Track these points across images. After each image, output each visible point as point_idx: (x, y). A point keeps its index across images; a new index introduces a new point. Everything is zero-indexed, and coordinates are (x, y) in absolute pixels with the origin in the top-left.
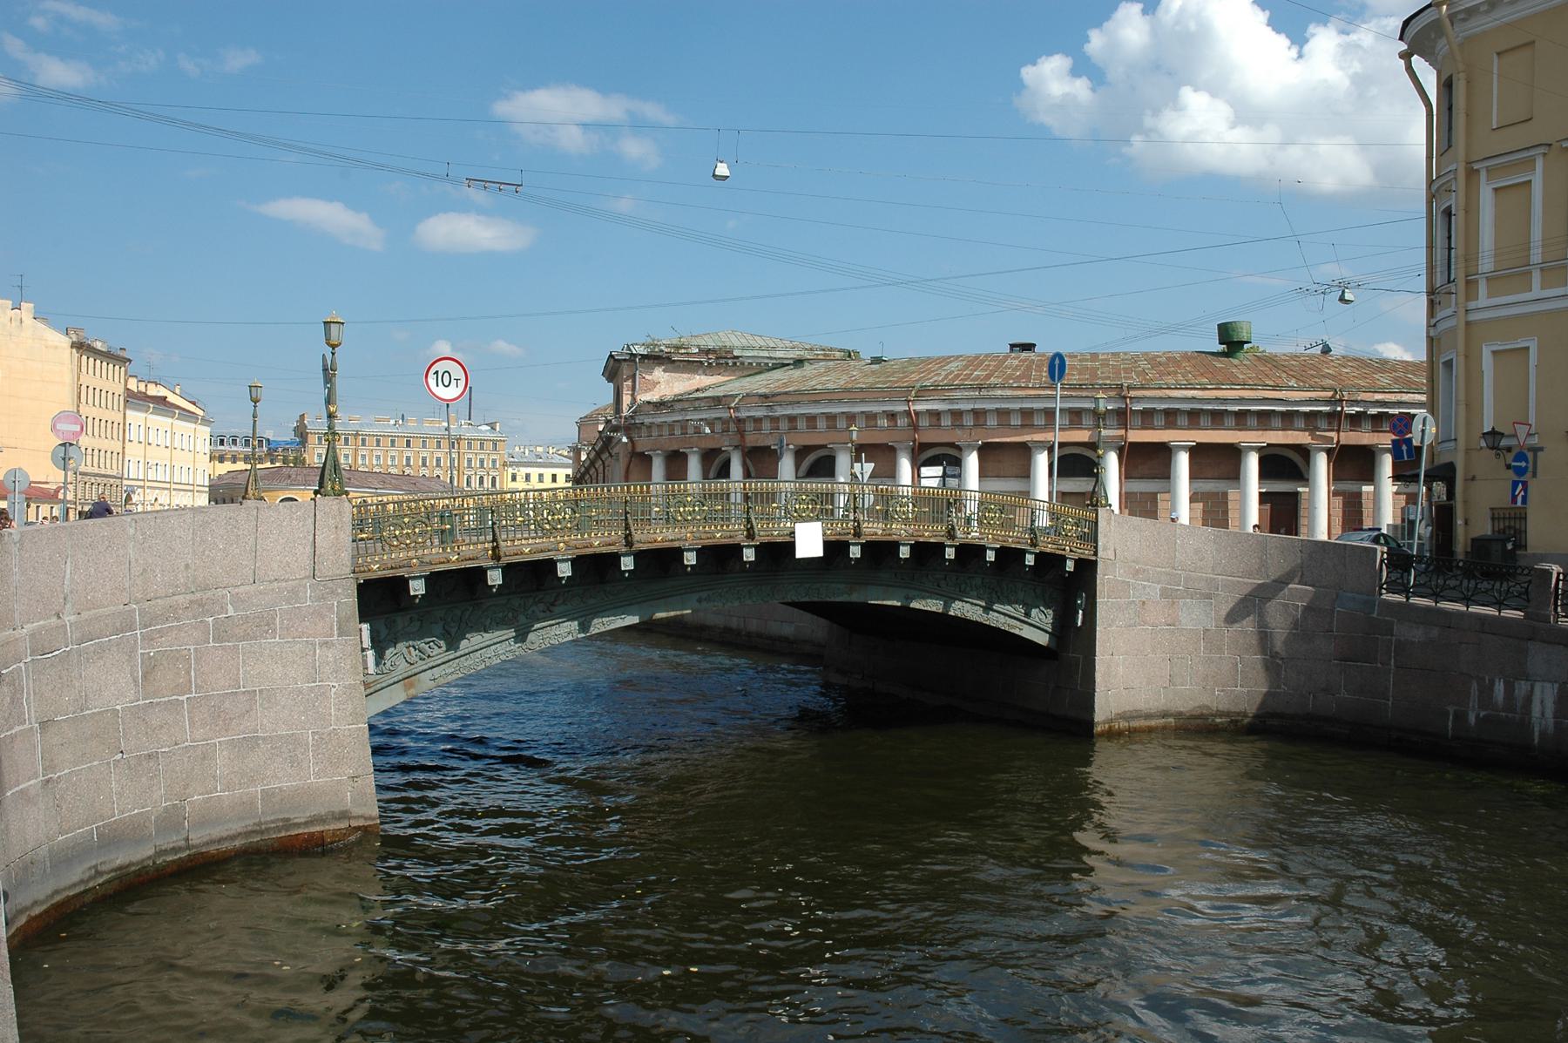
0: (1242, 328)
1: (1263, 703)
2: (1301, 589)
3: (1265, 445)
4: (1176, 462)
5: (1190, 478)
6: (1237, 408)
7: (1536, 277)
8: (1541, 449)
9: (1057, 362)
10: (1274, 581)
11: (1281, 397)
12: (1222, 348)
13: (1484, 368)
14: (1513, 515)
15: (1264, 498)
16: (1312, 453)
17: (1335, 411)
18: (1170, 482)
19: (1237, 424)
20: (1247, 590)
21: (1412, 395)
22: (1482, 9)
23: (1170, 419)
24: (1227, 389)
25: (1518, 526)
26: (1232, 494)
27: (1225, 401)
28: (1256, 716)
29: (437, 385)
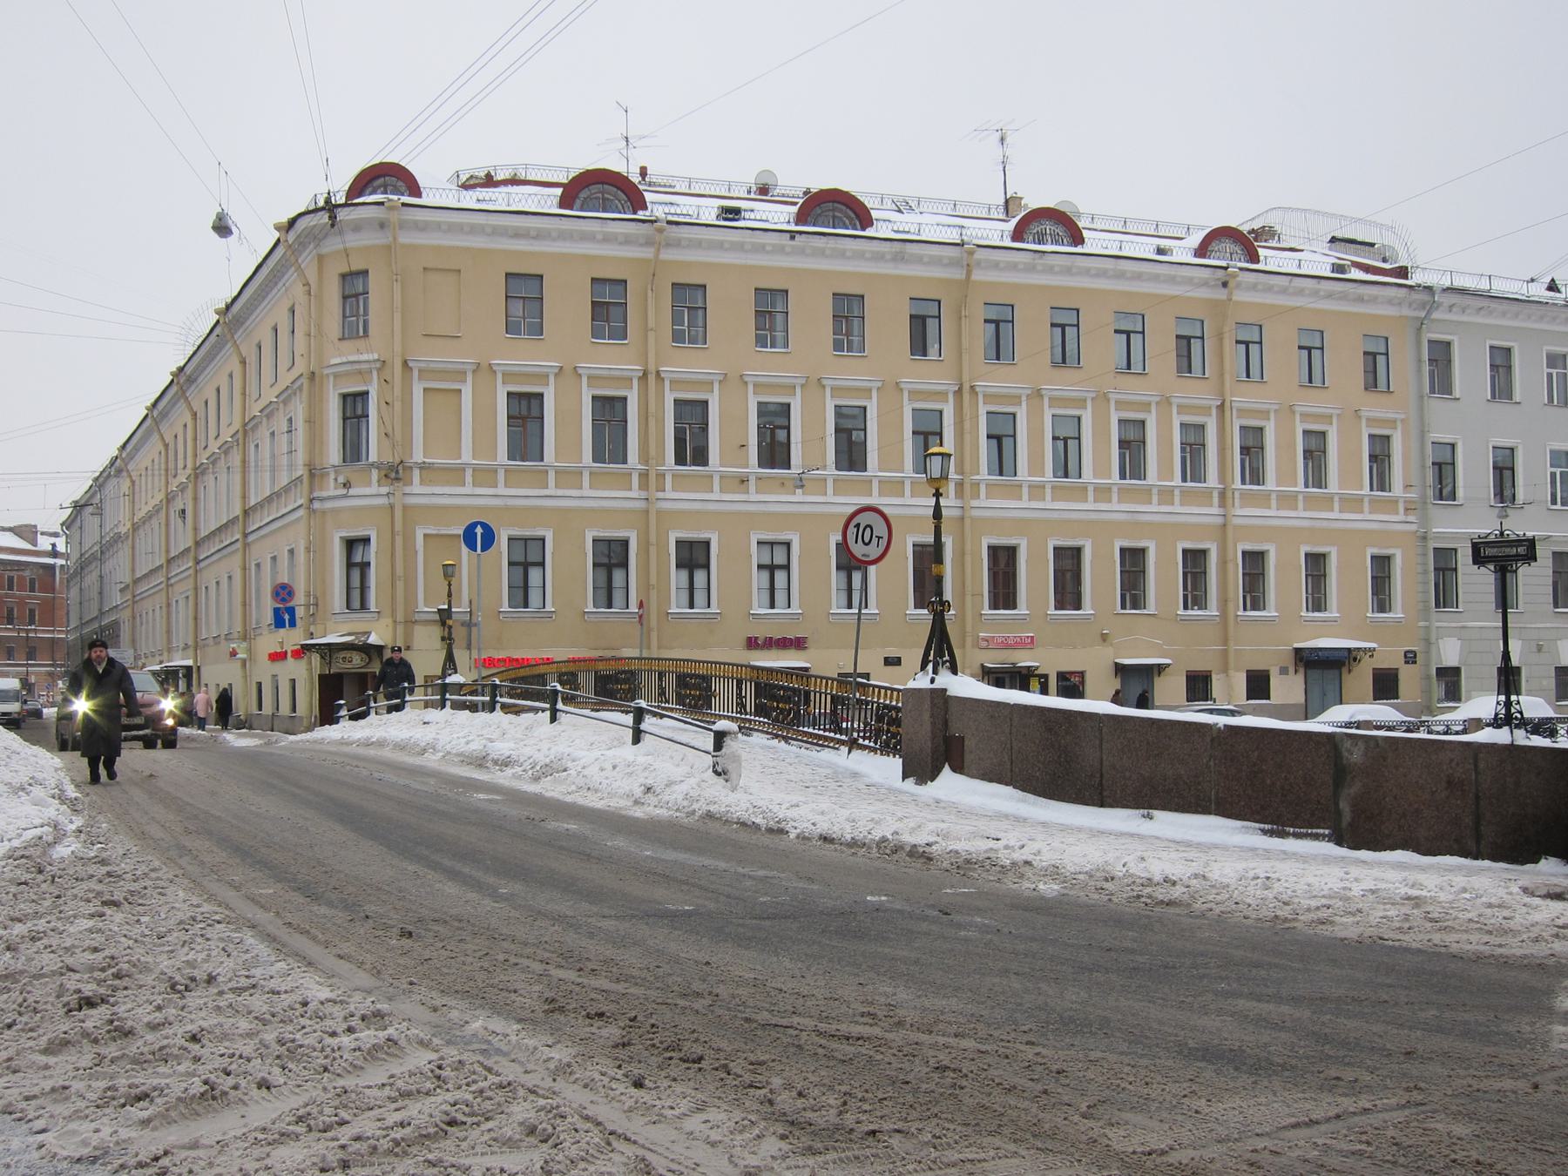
9: (479, 530)
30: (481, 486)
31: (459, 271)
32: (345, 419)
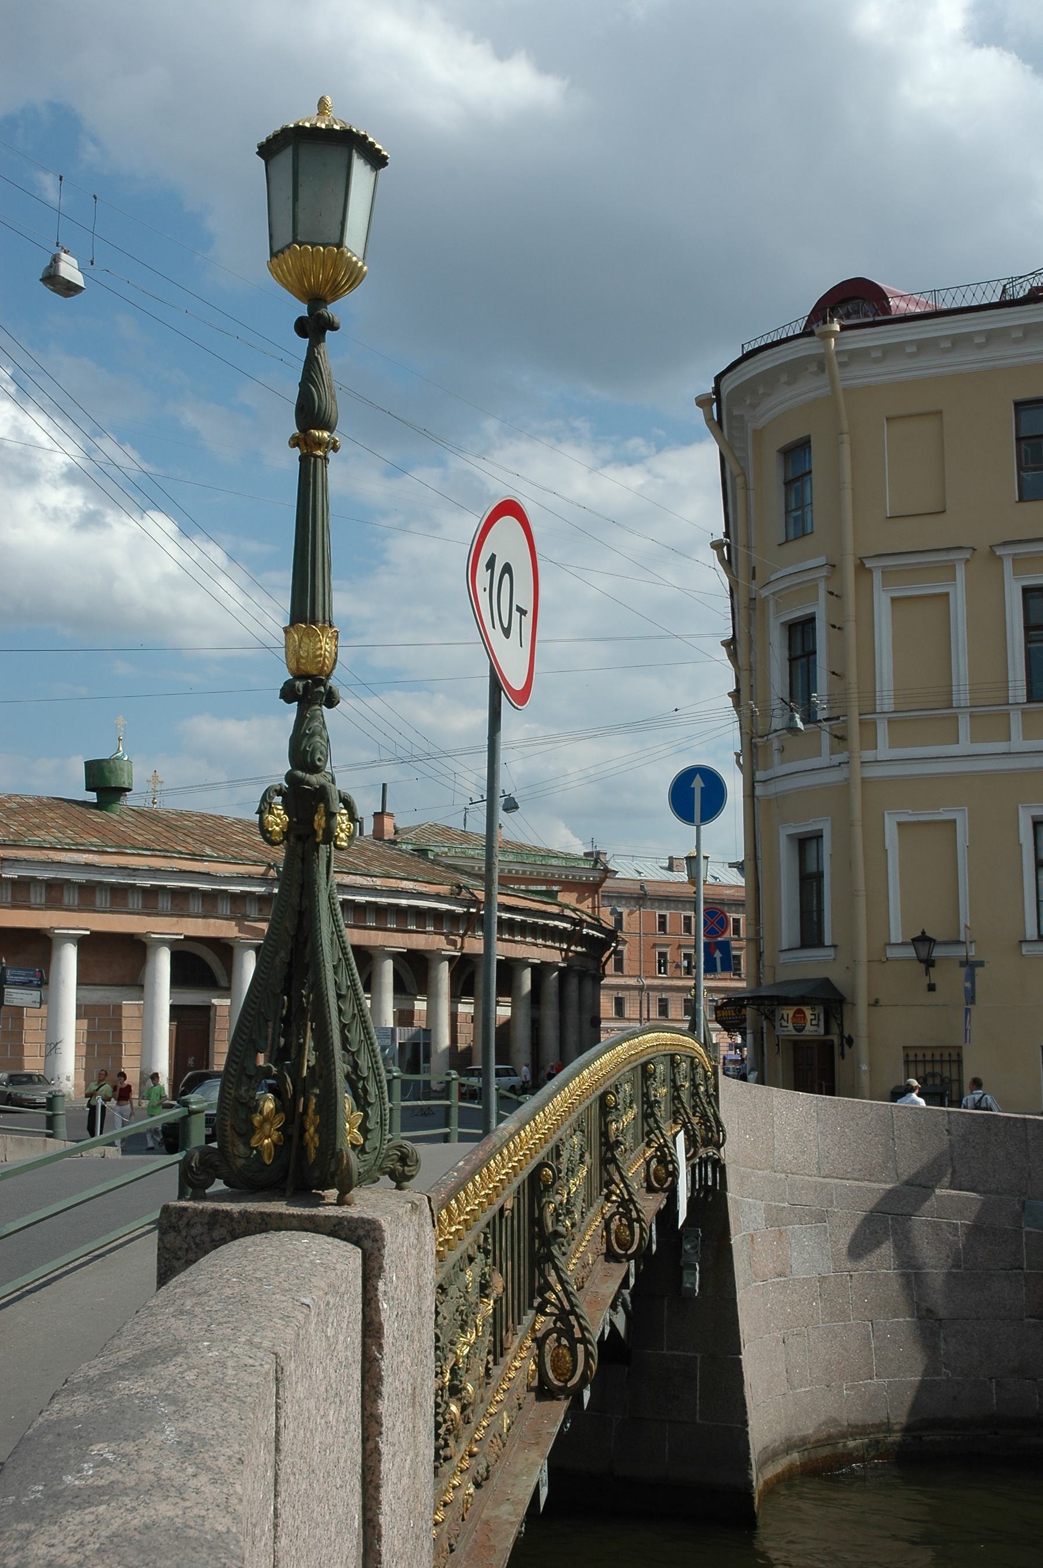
0: (122, 770)
1: (916, 1406)
2: (958, 1196)
3: (182, 937)
4: (59, 959)
5: (78, 984)
6: (148, 883)
7: (1016, 721)
8: (981, 964)
9: (698, 784)
10: (907, 1183)
11: (202, 870)
12: (92, 797)
13: (888, 844)
14: (929, 1058)
15: (83, 1011)
16: (236, 951)
17: (271, 894)
18: (143, 991)
19: (144, 907)
20: (870, 1204)
21: (354, 877)
22: (874, 355)
23: (54, 894)
24: (133, 854)
25: (946, 1074)
26: (129, 1006)
27: (135, 871)
28: (907, 1429)
29: (494, 627)
30: (985, 740)
31: (941, 412)
32: (792, 660)
